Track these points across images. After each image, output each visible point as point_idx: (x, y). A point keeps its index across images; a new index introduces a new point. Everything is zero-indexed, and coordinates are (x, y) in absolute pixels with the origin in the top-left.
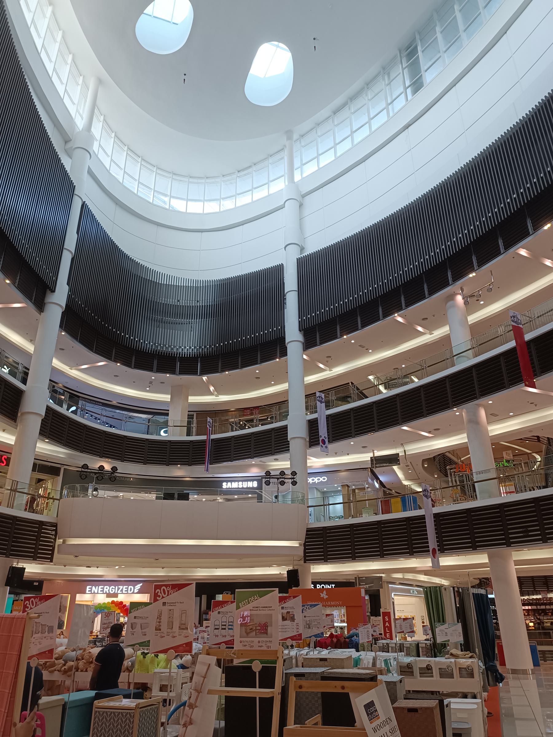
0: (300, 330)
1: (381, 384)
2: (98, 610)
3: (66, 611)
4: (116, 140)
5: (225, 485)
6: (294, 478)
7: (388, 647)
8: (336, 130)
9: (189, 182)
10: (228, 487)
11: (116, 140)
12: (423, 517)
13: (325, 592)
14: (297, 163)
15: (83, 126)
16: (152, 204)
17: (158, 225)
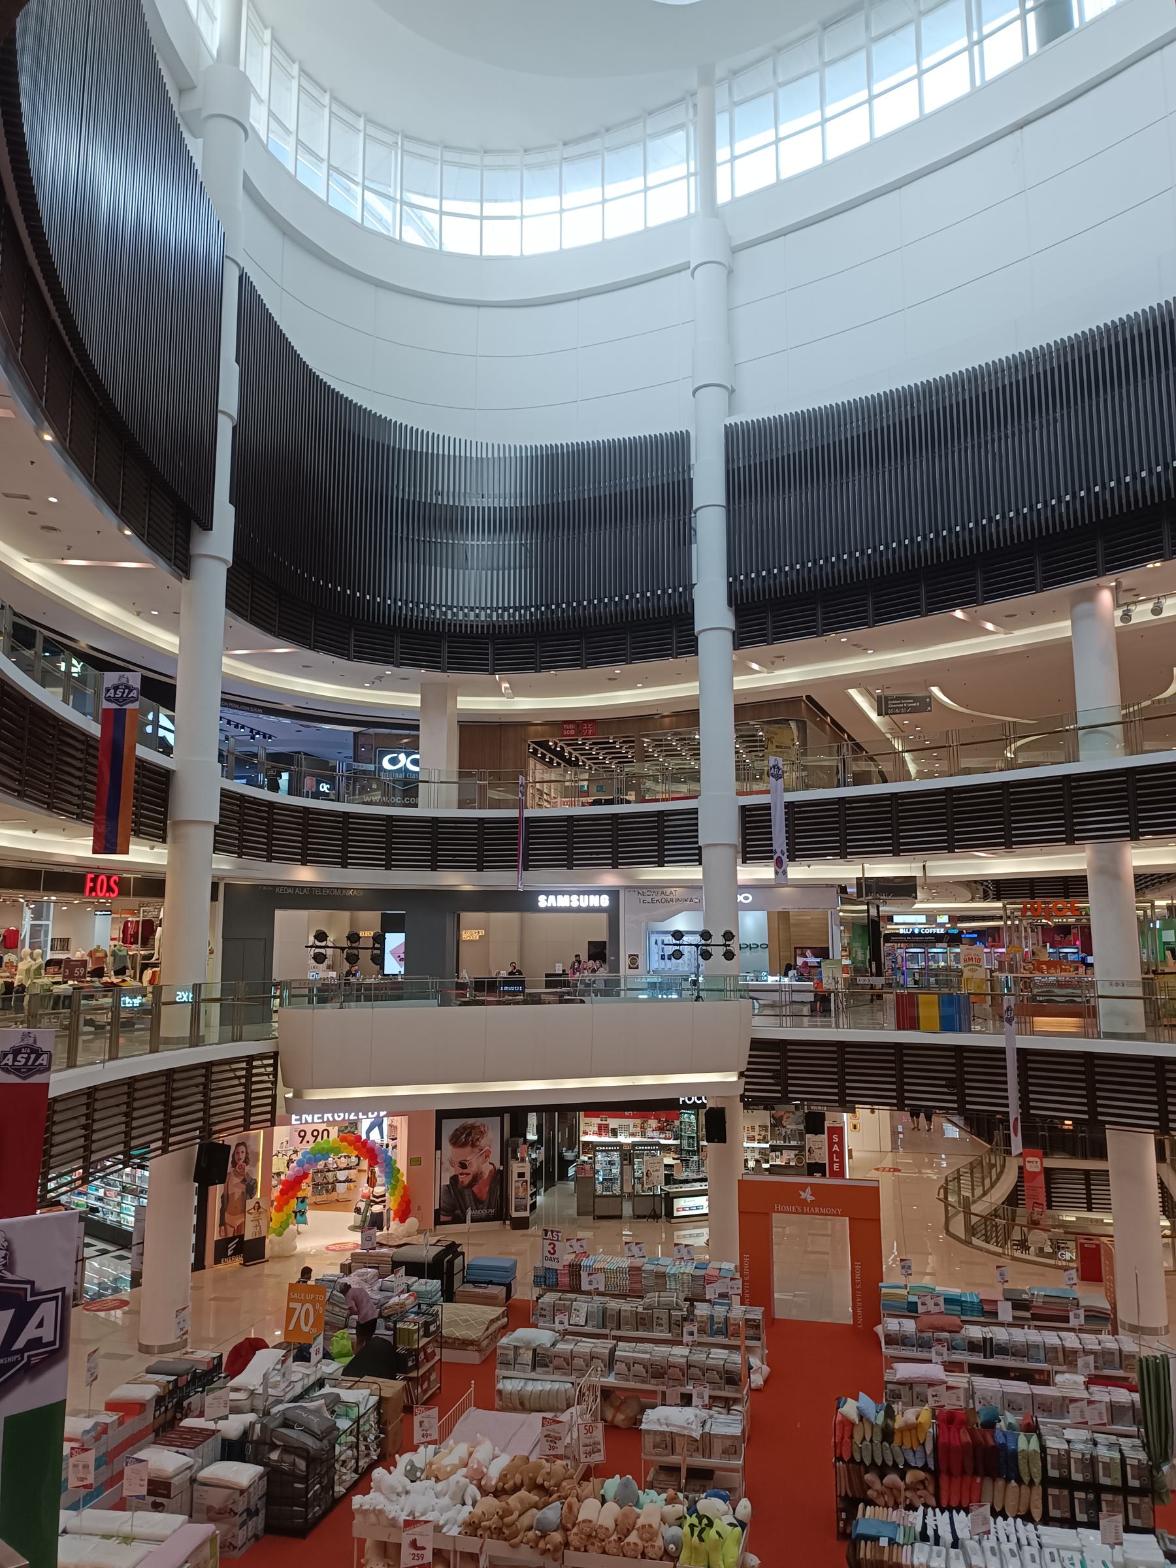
0: (730, 604)
1: (907, 751)
2: (318, 1155)
3: (258, 1160)
4: (276, 53)
5: (542, 901)
6: (729, 945)
7: (1069, 1458)
9: (444, 162)
10: (549, 905)
11: (276, 53)
12: (767, 807)
13: (808, 1190)
14: (722, 154)
15: (220, 43)
16: (361, 227)
17: (376, 286)
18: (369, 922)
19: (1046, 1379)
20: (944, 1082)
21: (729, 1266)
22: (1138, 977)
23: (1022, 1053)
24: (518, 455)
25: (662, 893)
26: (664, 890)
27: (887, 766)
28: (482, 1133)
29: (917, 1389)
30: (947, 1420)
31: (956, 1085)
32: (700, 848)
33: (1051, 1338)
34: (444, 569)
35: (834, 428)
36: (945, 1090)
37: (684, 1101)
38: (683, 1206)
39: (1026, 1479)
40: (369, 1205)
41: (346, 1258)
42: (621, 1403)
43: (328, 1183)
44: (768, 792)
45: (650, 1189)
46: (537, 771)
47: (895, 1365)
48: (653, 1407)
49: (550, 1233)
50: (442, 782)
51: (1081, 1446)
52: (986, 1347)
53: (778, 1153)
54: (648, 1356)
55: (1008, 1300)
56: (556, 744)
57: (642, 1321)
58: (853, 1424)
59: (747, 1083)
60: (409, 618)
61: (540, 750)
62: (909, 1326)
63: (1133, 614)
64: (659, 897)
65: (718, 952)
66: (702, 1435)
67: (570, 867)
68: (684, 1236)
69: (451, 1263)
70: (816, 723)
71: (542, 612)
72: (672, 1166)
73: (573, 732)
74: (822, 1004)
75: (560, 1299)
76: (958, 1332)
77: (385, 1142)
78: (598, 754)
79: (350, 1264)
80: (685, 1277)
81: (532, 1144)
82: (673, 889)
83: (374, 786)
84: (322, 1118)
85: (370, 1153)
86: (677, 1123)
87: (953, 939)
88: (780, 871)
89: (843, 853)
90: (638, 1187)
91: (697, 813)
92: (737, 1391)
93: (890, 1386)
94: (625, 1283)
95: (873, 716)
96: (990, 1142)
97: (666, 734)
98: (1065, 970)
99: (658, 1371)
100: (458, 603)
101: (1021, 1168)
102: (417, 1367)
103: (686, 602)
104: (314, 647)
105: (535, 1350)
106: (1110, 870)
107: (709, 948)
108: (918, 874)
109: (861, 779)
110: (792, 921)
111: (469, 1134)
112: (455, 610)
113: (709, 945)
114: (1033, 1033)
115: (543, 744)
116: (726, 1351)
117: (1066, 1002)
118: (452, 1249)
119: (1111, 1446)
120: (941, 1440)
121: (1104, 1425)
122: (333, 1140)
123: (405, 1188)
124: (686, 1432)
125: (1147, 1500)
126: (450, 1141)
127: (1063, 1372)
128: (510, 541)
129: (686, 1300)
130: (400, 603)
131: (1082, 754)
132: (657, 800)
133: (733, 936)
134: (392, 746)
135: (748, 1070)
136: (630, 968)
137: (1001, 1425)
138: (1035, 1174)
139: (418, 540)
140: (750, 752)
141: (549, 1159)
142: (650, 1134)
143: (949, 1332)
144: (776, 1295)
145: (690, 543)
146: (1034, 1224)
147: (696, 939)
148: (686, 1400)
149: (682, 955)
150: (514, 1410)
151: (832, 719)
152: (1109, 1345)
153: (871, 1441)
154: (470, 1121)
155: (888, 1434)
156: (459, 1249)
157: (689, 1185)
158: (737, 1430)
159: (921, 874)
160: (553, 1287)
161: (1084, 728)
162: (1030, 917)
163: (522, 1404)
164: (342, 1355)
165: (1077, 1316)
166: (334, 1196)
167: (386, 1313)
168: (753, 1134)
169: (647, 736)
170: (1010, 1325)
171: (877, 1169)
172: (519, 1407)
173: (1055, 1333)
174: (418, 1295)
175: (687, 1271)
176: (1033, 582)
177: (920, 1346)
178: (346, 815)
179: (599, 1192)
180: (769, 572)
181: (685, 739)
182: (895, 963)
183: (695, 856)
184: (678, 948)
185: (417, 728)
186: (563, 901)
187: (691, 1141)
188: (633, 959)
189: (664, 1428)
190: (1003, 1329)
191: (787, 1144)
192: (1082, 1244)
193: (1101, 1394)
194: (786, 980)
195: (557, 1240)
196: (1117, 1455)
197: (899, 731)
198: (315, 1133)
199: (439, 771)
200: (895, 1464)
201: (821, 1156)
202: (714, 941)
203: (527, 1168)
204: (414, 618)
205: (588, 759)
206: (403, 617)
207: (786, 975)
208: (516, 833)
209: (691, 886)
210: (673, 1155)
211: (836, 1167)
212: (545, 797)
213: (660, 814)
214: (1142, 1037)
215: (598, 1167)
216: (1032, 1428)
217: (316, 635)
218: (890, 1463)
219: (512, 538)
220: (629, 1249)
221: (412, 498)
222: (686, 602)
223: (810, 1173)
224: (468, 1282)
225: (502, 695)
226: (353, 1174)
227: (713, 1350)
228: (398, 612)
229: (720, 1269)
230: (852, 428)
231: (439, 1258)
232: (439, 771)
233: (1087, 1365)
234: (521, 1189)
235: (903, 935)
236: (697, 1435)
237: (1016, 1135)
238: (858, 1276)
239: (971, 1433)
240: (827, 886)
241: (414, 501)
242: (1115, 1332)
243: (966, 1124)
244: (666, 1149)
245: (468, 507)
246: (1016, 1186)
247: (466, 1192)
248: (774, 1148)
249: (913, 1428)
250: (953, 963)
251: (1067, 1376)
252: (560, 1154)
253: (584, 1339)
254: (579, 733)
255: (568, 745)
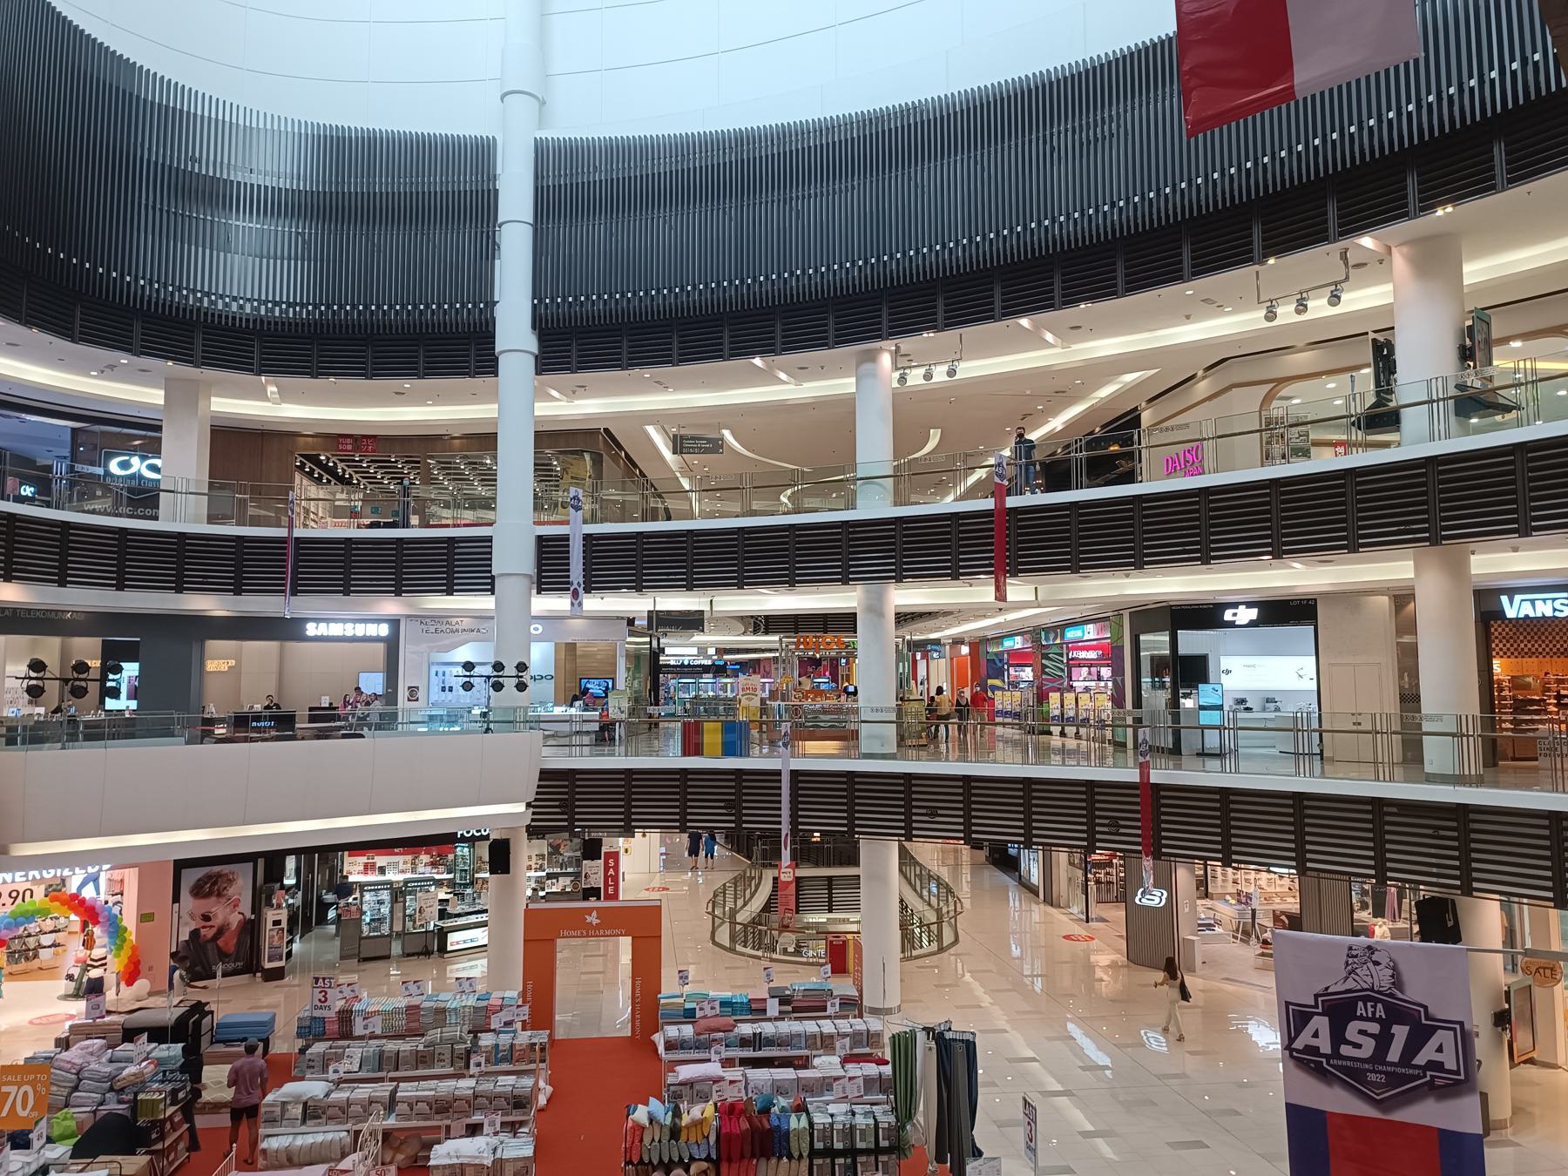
0: (534, 327)
2: (21, 919)
5: (311, 629)
6: (522, 677)
7: (832, 1129)
8: (1057, 423)
10: (319, 634)
12: (566, 538)
13: (594, 914)
18: (88, 649)
19: (805, 1063)
20: (723, 804)
21: (513, 994)
22: (893, 703)
23: (795, 774)
24: (296, 131)
25: (448, 623)
26: (450, 620)
27: (672, 504)
28: (231, 882)
29: (697, 1087)
30: (729, 1111)
31: (734, 806)
32: (493, 578)
33: (810, 1027)
34: (208, 251)
35: (647, 160)
36: (724, 811)
37: (462, 835)
38: (455, 940)
39: (796, 1154)
40: (85, 970)
41: (63, 1030)
42: (401, 1144)
43: (29, 950)
44: (567, 523)
45: (422, 926)
46: (304, 488)
47: (678, 1068)
48: (439, 1142)
49: (321, 980)
50: (190, 493)
51: (842, 1118)
52: (756, 1041)
53: (554, 881)
54: (433, 1093)
55: (773, 997)
56: (328, 459)
57: (422, 1059)
58: (643, 1128)
59: (534, 813)
60: (154, 300)
61: (308, 464)
62: (688, 1031)
63: (908, 378)
64: (444, 627)
65: (510, 684)
66: (493, 1162)
67: (347, 593)
68: (457, 970)
69: (198, 1024)
70: (611, 456)
71: (321, 312)
72: (447, 900)
73: (349, 447)
74: (604, 735)
75: (331, 1048)
76: (731, 1031)
77: (103, 897)
78: (376, 472)
79: (67, 1038)
80: (467, 1010)
81: (288, 889)
82: (459, 619)
83: (99, 493)
84: (26, 876)
85: (90, 914)
86: (451, 857)
87: (718, 670)
88: (576, 602)
89: (638, 587)
90: (409, 924)
91: (491, 541)
92: (524, 1114)
93: (672, 1088)
94: (401, 1023)
95: (668, 455)
96: (750, 858)
97: (454, 456)
98: (829, 698)
99: (442, 1107)
100: (231, 291)
101: (775, 879)
102: (162, 1138)
103: (486, 319)
104: (28, 322)
105: (305, 1104)
106: (876, 610)
107: (501, 680)
108: (706, 608)
109: (652, 515)
110: (578, 653)
111: (215, 883)
112: (213, 297)
113: (501, 676)
114: (804, 756)
115: (314, 459)
116: (514, 1077)
117: (830, 727)
118: (199, 1009)
119: (866, 1114)
120: (723, 1131)
121: (862, 1096)
122: (41, 901)
123: (134, 949)
124: (477, 1161)
125: (894, 1156)
126: (191, 892)
127: (820, 1056)
128: (285, 228)
129: (469, 1032)
130: (142, 282)
131: (859, 502)
132: (447, 526)
133: (527, 668)
134: (122, 446)
135: (536, 800)
136: (409, 700)
137: (775, 1110)
138: (789, 883)
139: (168, 212)
140: (542, 481)
141: (306, 903)
142: (421, 869)
143: (724, 1032)
144: (557, 1017)
145: (493, 258)
146: (785, 928)
147: (488, 671)
148: (474, 1130)
149: (473, 686)
150: (281, 1167)
151: (626, 453)
152: (858, 1028)
153: (660, 1141)
154: (216, 869)
155: (675, 1132)
156: (207, 1008)
157: (464, 918)
158: (528, 1151)
159: (709, 609)
160: (320, 1037)
161: (862, 479)
162: (802, 650)
163: (290, 1160)
164: (62, 1138)
165: (833, 1005)
166: (35, 964)
167: (118, 1086)
168: (530, 863)
169: (431, 457)
170: (776, 1019)
171: (648, 890)
172: (287, 1163)
173: (814, 1022)
174: (159, 1062)
175: (469, 1004)
176: (826, 338)
177: (697, 1048)
178: (66, 525)
179: (365, 934)
180: (575, 299)
181: (475, 463)
182: (668, 693)
183: (488, 585)
184: (468, 679)
185: (159, 429)
186: (336, 630)
187: (464, 874)
188: (413, 691)
189: (455, 1161)
190: (769, 1024)
191: (564, 871)
192: (831, 942)
193: (853, 1070)
194: (573, 711)
195: (330, 987)
196: (871, 1121)
197: (688, 470)
198: (14, 894)
199: (188, 481)
200: (681, 1159)
201: (597, 880)
202: (506, 672)
203: (283, 915)
204: (161, 302)
205: (363, 478)
206: (146, 299)
207: (571, 706)
208: (284, 554)
209: (482, 617)
210: (445, 889)
211: (610, 891)
212: (312, 516)
213: (451, 541)
214: (892, 757)
215: (365, 908)
216: (801, 1108)
217: (28, 308)
218: (676, 1159)
219: (287, 225)
220: (407, 989)
221: (160, 161)
222: (486, 319)
223: (586, 898)
224: (218, 1042)
225: (266, 399)
226: (60, 937)
227: (500, 1078)
228: (139, 292)
229: (503, 998)
230: (659, 164)
231: (182, 1021)
232: (188, 481)
233: (843, 1047)
234: (276, 938)
235: (673, 666)
236: (488, 1162)
237: (786, 849)
238: (638, 991)
239: (750, 1120)
240: (618, 618)
241: (163, 165)
242: (861, 1016)
243: (726, 842)
244: (439, 883)
245: (232, 182)
246: (770, 899)
247: (209, 946)
248: (549, 876)
249: (698, 1124)
250: (721, 693)
251: (823, 1058)
252: (319, 897)
253: (361, 1085)
254: (356, 449)
255: (341, 461)
